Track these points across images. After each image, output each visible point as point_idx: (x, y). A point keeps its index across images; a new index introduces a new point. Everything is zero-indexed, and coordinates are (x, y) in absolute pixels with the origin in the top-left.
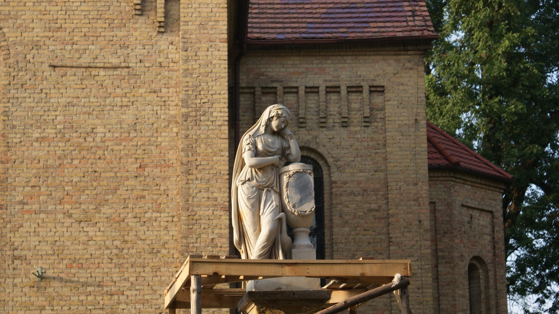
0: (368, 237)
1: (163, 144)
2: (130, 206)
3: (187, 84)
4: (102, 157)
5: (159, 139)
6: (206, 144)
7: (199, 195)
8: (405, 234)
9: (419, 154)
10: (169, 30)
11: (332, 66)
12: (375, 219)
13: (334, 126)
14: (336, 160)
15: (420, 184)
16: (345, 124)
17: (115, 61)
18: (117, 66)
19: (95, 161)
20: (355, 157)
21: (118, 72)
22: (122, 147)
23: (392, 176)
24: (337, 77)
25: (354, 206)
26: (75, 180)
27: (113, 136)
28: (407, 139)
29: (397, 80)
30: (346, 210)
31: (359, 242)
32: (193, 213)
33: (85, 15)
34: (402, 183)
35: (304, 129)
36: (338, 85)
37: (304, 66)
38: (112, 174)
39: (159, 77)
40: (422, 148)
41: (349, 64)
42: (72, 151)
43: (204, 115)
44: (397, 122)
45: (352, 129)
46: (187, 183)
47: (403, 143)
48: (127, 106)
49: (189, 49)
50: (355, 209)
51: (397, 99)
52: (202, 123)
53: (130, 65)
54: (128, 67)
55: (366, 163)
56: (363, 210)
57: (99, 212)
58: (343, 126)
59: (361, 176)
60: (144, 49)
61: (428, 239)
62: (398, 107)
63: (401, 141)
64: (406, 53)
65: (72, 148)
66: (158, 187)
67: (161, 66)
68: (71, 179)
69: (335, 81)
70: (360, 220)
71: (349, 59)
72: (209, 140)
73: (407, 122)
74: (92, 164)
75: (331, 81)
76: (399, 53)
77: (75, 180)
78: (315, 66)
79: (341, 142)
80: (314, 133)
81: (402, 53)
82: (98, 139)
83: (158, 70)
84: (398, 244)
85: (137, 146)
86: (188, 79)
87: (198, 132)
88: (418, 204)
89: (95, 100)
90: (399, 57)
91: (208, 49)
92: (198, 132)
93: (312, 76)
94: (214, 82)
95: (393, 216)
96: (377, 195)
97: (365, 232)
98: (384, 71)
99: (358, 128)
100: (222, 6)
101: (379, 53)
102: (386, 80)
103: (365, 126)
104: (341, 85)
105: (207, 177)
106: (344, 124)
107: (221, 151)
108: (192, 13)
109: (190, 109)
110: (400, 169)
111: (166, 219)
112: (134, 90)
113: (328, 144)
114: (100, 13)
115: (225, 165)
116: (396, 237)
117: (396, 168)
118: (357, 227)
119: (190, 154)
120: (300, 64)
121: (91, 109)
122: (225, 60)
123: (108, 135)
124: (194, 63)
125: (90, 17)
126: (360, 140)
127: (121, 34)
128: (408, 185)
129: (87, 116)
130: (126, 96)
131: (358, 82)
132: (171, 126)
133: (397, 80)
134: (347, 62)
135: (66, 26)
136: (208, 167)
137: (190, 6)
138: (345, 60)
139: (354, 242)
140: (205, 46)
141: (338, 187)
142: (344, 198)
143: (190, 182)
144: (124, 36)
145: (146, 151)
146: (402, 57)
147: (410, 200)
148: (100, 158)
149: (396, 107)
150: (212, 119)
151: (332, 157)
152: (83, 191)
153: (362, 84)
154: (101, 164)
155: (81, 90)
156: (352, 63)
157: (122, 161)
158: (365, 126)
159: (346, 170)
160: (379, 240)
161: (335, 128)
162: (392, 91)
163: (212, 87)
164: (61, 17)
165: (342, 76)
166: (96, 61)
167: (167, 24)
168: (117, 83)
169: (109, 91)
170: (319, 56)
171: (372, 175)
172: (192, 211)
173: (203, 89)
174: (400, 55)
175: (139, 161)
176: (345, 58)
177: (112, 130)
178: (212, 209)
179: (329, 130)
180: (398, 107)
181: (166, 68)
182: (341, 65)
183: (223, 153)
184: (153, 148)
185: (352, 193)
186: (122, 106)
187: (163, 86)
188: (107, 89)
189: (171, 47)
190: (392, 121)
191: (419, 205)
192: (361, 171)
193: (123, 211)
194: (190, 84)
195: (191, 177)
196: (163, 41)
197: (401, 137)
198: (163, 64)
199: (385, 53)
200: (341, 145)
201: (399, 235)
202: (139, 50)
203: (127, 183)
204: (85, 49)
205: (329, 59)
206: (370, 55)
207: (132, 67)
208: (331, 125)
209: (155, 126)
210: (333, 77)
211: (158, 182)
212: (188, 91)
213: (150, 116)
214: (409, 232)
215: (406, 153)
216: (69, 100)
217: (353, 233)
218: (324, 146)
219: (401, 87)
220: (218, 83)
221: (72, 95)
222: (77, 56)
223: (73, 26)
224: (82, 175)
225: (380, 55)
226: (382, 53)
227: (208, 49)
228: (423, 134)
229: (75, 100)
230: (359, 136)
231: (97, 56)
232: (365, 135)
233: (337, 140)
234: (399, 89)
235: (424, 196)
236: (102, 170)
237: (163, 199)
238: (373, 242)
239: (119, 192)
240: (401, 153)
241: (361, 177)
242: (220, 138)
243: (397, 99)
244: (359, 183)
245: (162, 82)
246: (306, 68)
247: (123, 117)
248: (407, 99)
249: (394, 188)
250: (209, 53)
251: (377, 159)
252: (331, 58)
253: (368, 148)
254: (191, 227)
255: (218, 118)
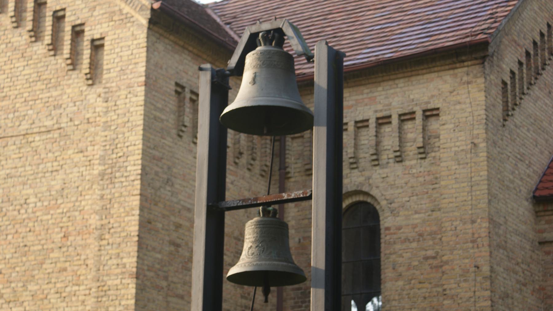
0: (424, 290)
1: (86, 208)
2: (53, 280)
3: (105, 138)
4: (32, 229)
5: (83, 203)
6: (119, 203)
7: (110, 262)
8: (461, 285)
9: (478, 184)
10: (97, 81)
11: (383, 93)
12: (431, 268)
13: (388, 163)
14: (389, 202)
15: (479, 220)
16: (399, 159)
17: (49, 123)
18: (50, 129)
19: (25, 234)
20: (410, 197)
21: (50, 136)
22: (49, 217)
23: (446, 215)
24: (388, 105)
25: (409, 255)
26: (8, 257)
27: (43, 205)
28: (464, 168)
29: (454, 99)
30: (400, 260)
31: (414, 297)
32: (103, 284)
33: (27, 79)
34: (458, 223)
35: (356, 171)
36: (389, 115)
37: (354, 98)
38: (40, 247)
39: (86, 134)
40: (481, 176)
41: (401, 88)
42: (7, 226)
43: (119, 171)
44: (453, 149)
45: (407, 163)
46: (99, 250)
47: (459, 174)
48: (57, 171)
49: (110, 99)
50: (410, 258)
51: (453, 121)
52: (116, 180)
53: (62, 125)
54: (60, 129)
55: (423, 202)
56: (419, 258)
57: (26, 290)
58: (398, 162)
59: (417, 218)
60: (75, 106)
61: (488, 288)
62: (454, 130)
63: (458, 171)
64: (462, 64)
65: (7, 223)
66: (78, 257)
67: (88, 123)
68: (4, 256)
69: (386, 110)
70: (415, 271)
71: (401, 83)
72: (122, 199)
73: (465, 147)
74: (23, 238)
75: (381, 111)
76: (454, 66)
77: (8, 257)
78: (365, 96)
79: (395, 181)
80: (367, 173)
81: (458, 65)
82: (30, 210)
83: (86, 126)
84: (452, 297)
85: (63, 213)
86: (106, 133)
87: (113, 191)
88: (476, 246)
89: (29, 168)
90: (456, 71)
91: (127, 96)
92: (113, 191)
93: (362, 108)
94: (130, 133)
95: (447, 263)
96: (434, 239)
97: (421, 285)
98: (439, 90)
99: (414, 162)
100: (141, 45)
101: (432, 70)
102: (441, 100)
103: (421, 158)
104: (392, 114)
105: (118, 240)
106: (398, 159)
107: (132, 209)
108: (114, 59)
109: (107, 166)
110: (457, 205)
111: (83, 293)
112: (64, 153)
113: (381, 185)
114: (39, 74)
115: (135, 225)
116: (450, 289)
117: (451, 205)
118: (411, 280)
119: (104, 217)
120: (350, 96)
121: (26, 178)
122: (141, 106)
123: (39, 204)
124: (113, 113)
125: (31, 80)
126: (416, 175)
127: (55, 94)
128: (465, 223)
129: (21, 187)
130: (56, 160)
131: (410, 107)
132: (94, 187)
133: (454, 99)
134: (400, 85)
135: (11, 93)
136: (119, 230)
137: (113, 52)
138: (397, 84)
139: (408, 298)
140: (123, 93)
141: (392, 234)
142: (398, 247)
143: (102, 248)
144: (58, 96)
145: (71, 218)
146: (460, 70)
147: (467, 242)
148: (30, 231)
149: (452, 131)
150: (125, 174)
151: (385, 199)
152: (14, 268)
153: (415, 109)
154: (31, 237)
155: (18, 160)
156: (404, 86)
157: (50, 231)
158: (421, 158)
159: (401, 213)
160: (436, 294)
161: (389, 165)
162: (447, 112)
163: (128, 137)
164: (6, 85)
165: (394, 104)
166: (33, 126)
167: (94, 75)
168: (49, 146)
169: (42, 156)
170: (369, 84)
171: (429, 215)
172: (103, 281)
173: (119, 142)
174: (456, 68)
175: (64, 230)
176: (397, 81)
177: (42, 199)
178: (120, 277)
179: (383, 168)
180: (454, 130)
181: (93, 124)
182: (392, 91)
183: (134, 212)
184: (77, 213)
185: (407, 240)
186: (52, 172)
187: (89, 144)
188: (40, 155)
189: (98, 99)
190: (447, 148)
191: (478, 247)
192: (416, 213)
193: (46, 286)
194: (108, 138)
195: (104, 242)
196: (93, 95)
197: (457, 167)
198: (91, 120)
199: (439, 68)
200: (395, 184)
201: (454, 286)
202: (71, 109)
203: (52, 255)
204: (25, 116)
205: (380, 86)
206: (423, 74)
207: (63, 128)
208: (384, 162)
209: (80, 189)
210: (383, 106)
211: (79, 252)
212: (105, 146)
213: (76, 179)
214: (465, 281)
215: (463, 185)
216: (8, 171)
217: (407, 287)
218: (377, 187)
219: (458, 107)
220: (134, 133)
221: (10, 166)
222: (17, 124)
223: (16, 92)
224: (14, 250)
225: (435, 72)
226: (436, 69)
227: (127, 96)
228: (482, 159)
229: (13, 170)
230: (414, 171)
231: (34, 121)
232: (422, 169)
233: (391, 179)
234: (455, 109)
235: (483, 235)
236: (31, 243)
237: (82, 270)
238: (429, 296)
239: (44, 266)
240: (457, 186)
241: (416, 219)
242: (133, 195)
243: (453, 121)
244: (415, 226)
245: (89, 139)
246: (356, 100)
247: (53, 183)
248: (464, 119)
249: (449, 229)
250: (127, 101)
251: (434, 196)
252: (382, 84)
253: (424, 184)
254: (99, 299)
255: (132, 172)
